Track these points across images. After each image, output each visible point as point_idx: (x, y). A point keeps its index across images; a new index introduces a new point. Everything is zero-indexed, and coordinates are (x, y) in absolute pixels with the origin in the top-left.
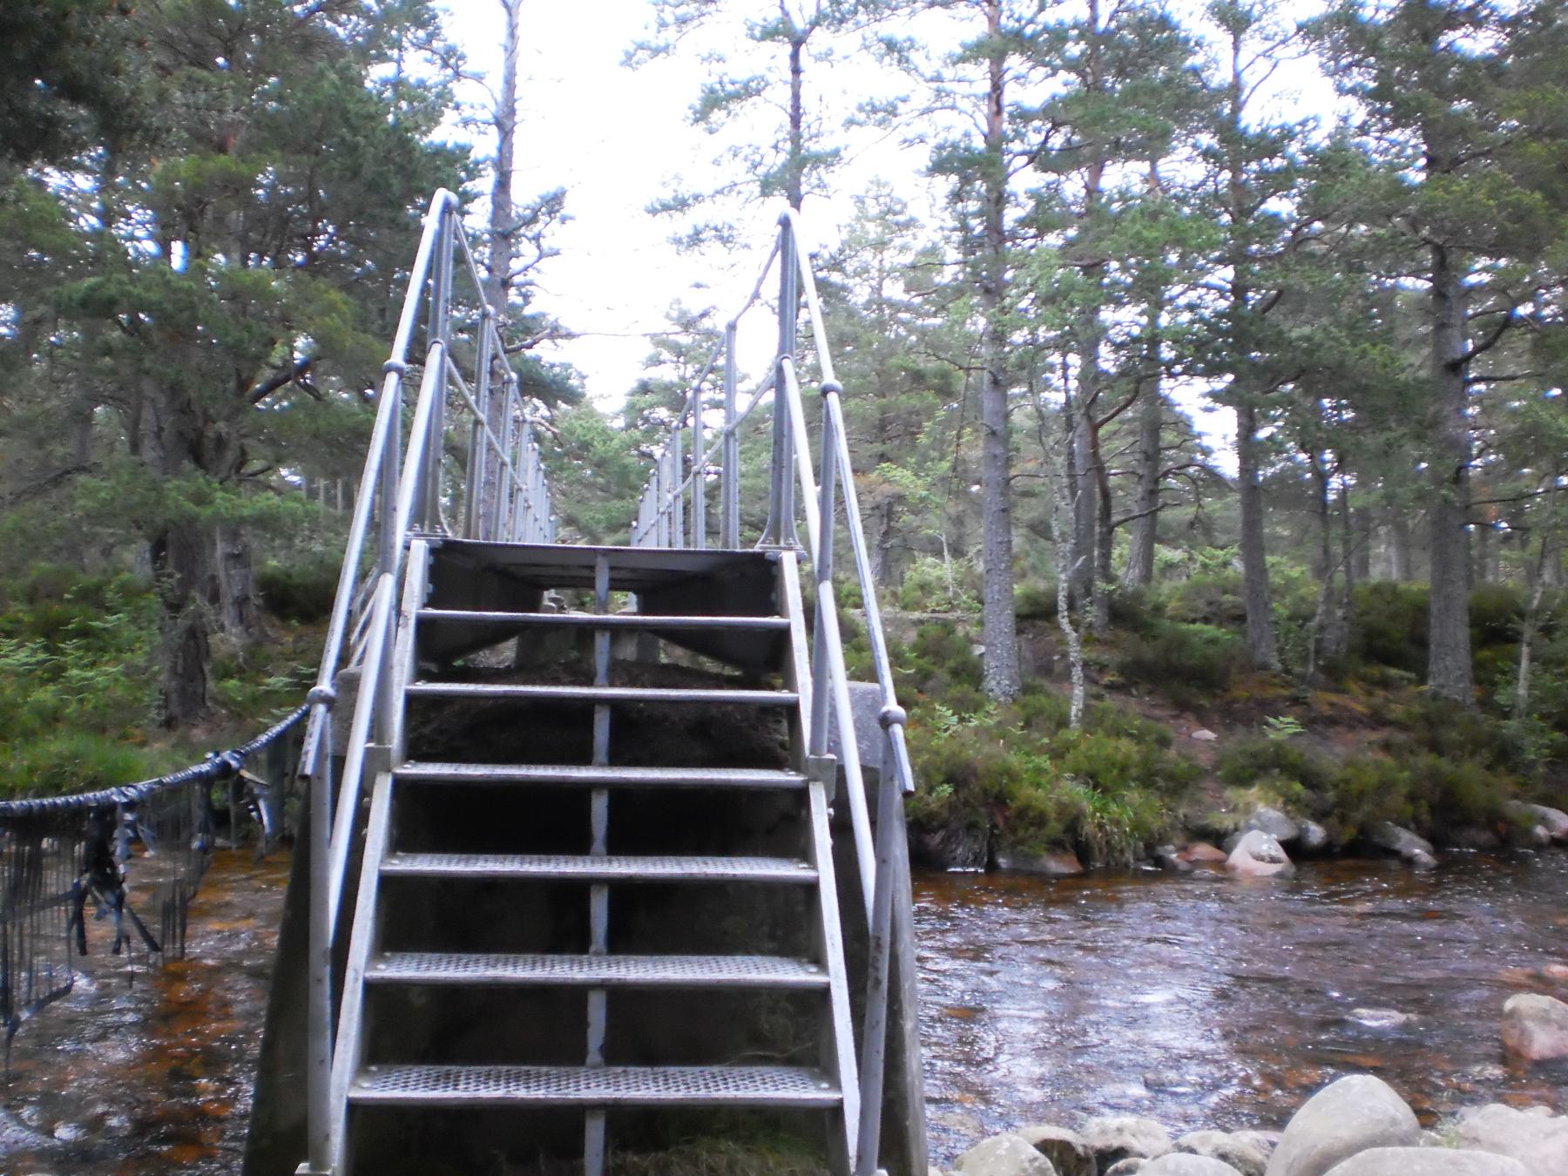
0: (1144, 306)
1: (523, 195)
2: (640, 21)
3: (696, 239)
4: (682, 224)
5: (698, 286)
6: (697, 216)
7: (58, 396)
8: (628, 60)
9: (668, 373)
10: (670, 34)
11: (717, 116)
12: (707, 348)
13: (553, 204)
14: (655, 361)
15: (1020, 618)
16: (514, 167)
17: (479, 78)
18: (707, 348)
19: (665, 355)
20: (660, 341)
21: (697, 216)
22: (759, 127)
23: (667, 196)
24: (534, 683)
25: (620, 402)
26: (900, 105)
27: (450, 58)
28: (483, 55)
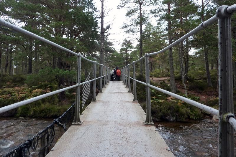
0: (111, 46)
1: (105, 26)
2: (119, 3)
3: (128, 32)
4: (125, 30)
5: (129, 37)
6: (128, 28)
7: (79, 4)
8: (118, 8)
9: (124, 47)
10: (124, 4)
11: (130, 15)
12: (128, 44)
13: (109, 27)
14: (123, 46)
15: (175, 80)
16: (104, 23)
17: (99, 11)
18: (128, 44)
19: (124, 45)
20: (123, 43)
21: (128, 28)
22: (136, 15)
23: (124, 26)
24: (27, 33)
25: (120, 51)
26: (150, 13)
27: (94, 9)
28: (99, 8)
